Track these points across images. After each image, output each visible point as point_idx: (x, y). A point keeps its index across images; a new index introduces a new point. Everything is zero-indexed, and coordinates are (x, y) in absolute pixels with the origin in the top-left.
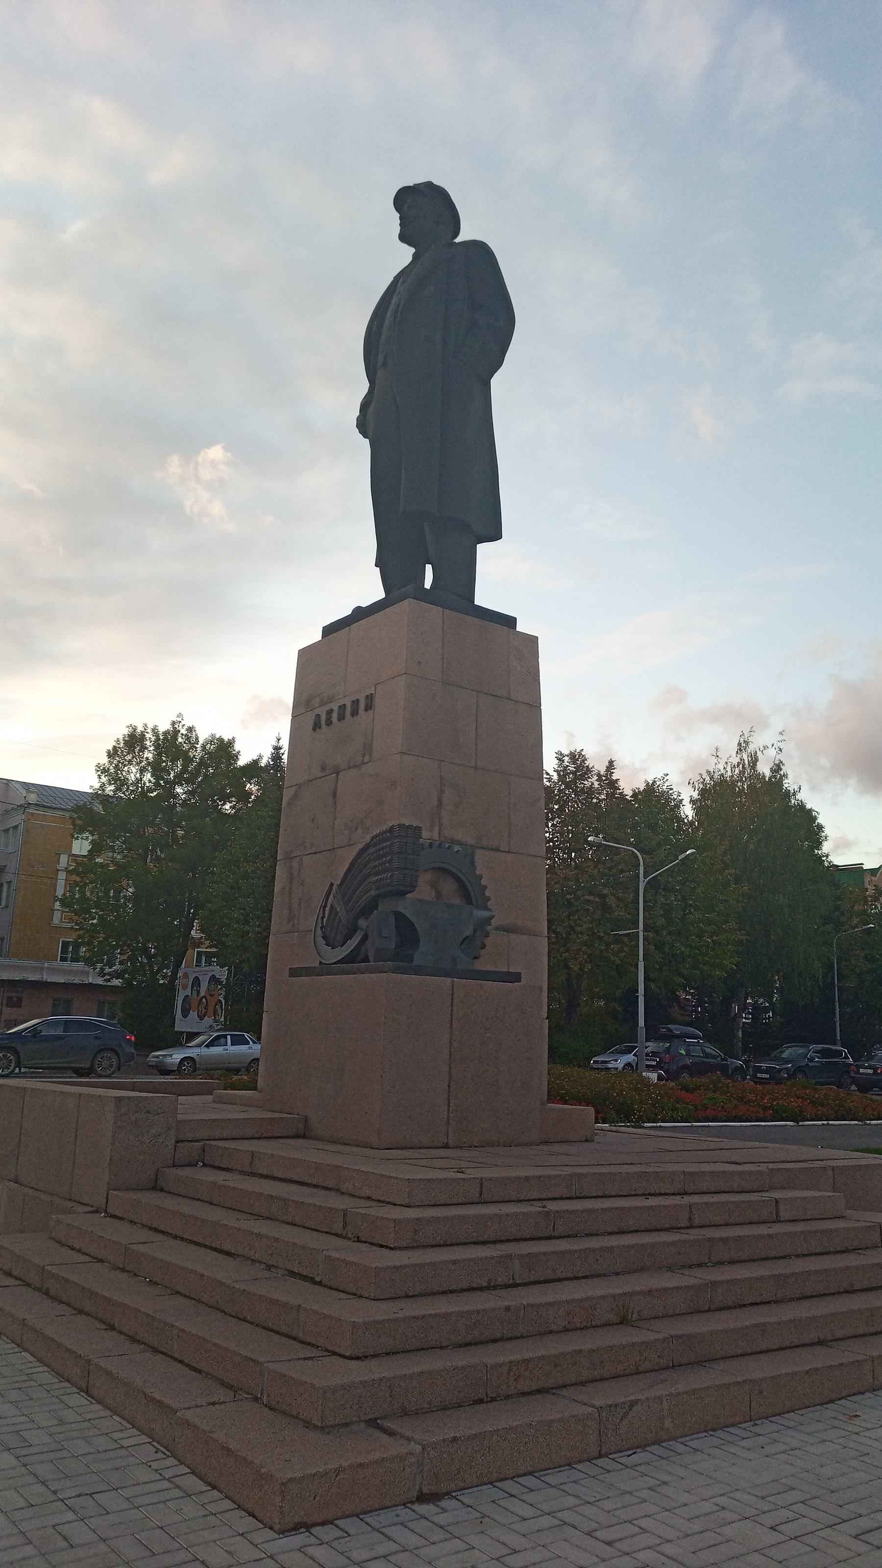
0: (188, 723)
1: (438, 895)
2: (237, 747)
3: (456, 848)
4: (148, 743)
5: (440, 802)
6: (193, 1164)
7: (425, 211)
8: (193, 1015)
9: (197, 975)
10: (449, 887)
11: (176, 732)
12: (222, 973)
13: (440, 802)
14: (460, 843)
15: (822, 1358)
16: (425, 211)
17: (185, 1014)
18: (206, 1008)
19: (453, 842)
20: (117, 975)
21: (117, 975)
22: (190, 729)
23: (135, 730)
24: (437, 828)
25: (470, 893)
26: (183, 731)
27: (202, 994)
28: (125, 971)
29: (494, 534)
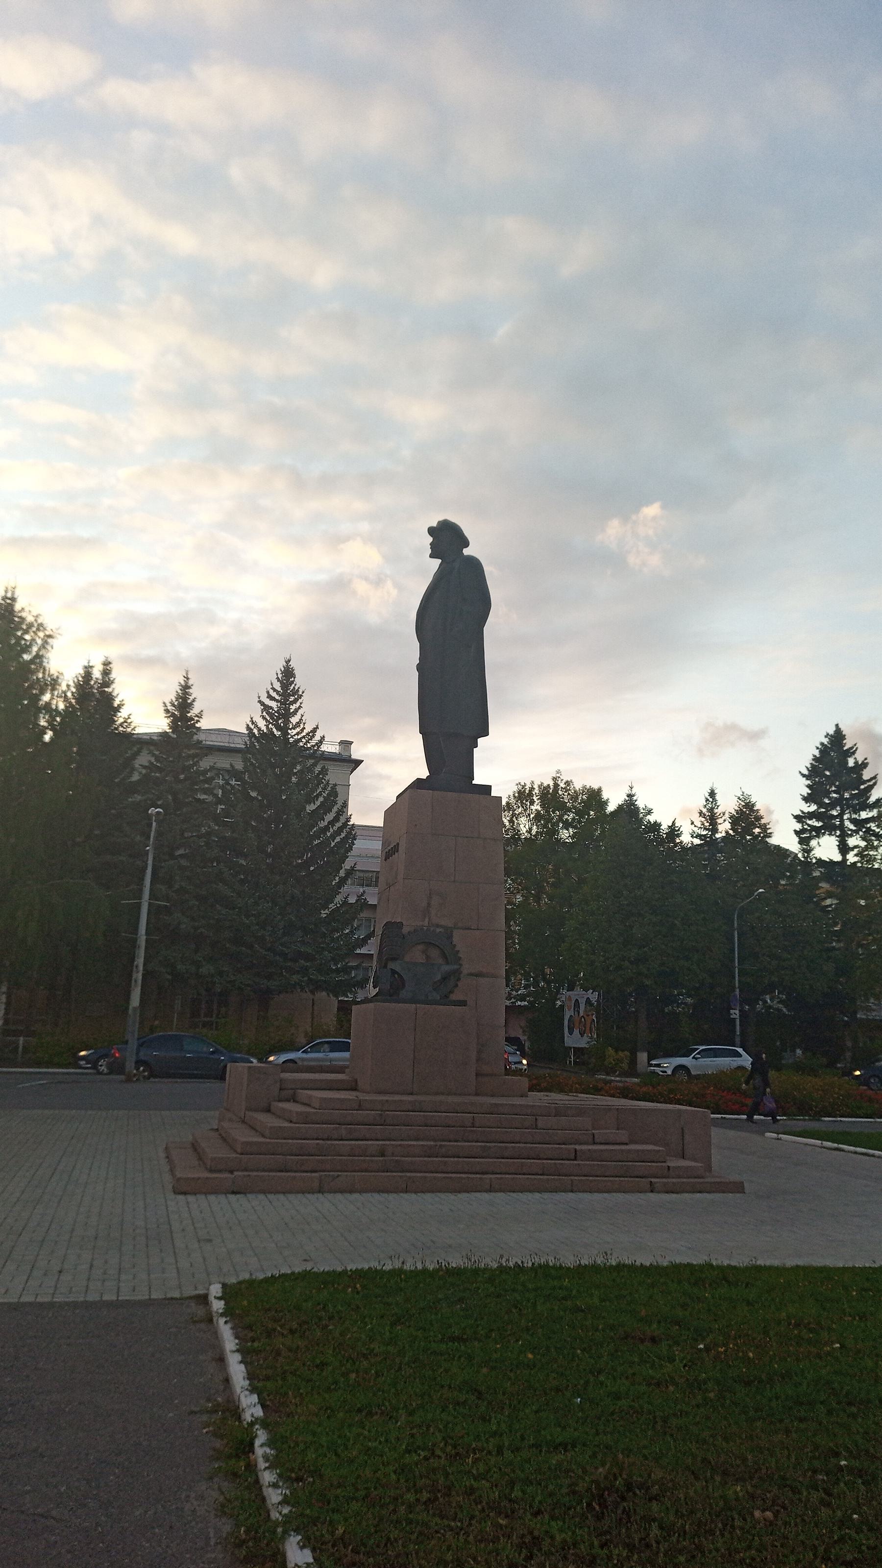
0: (566, 778)
1: (428, 957)
2: (605, 796)
3: (438, 930)
4: (535, 798)
5: (429, 905)
6: (288, 1101)
7: (447, 539)
8: (576, 1031)
9: (577, 997)
10: (434, 953)
11: (556, 785)
12: (594, 997)
13: (429, 905)
14: (441, 926)
15: (444, 1175)
16: (447, 539)
17: (571, 1032)
18: (585, 1026)
19: (438, 926)
20: (522, 998)
21: (522, 998)
22: (568, 783)
23: (523, 787)
24: (427, 920)
25: (450, 955)
26: (562, 785)
27: (581, 1014)
28: (528, 995)
29: (485, 733)
